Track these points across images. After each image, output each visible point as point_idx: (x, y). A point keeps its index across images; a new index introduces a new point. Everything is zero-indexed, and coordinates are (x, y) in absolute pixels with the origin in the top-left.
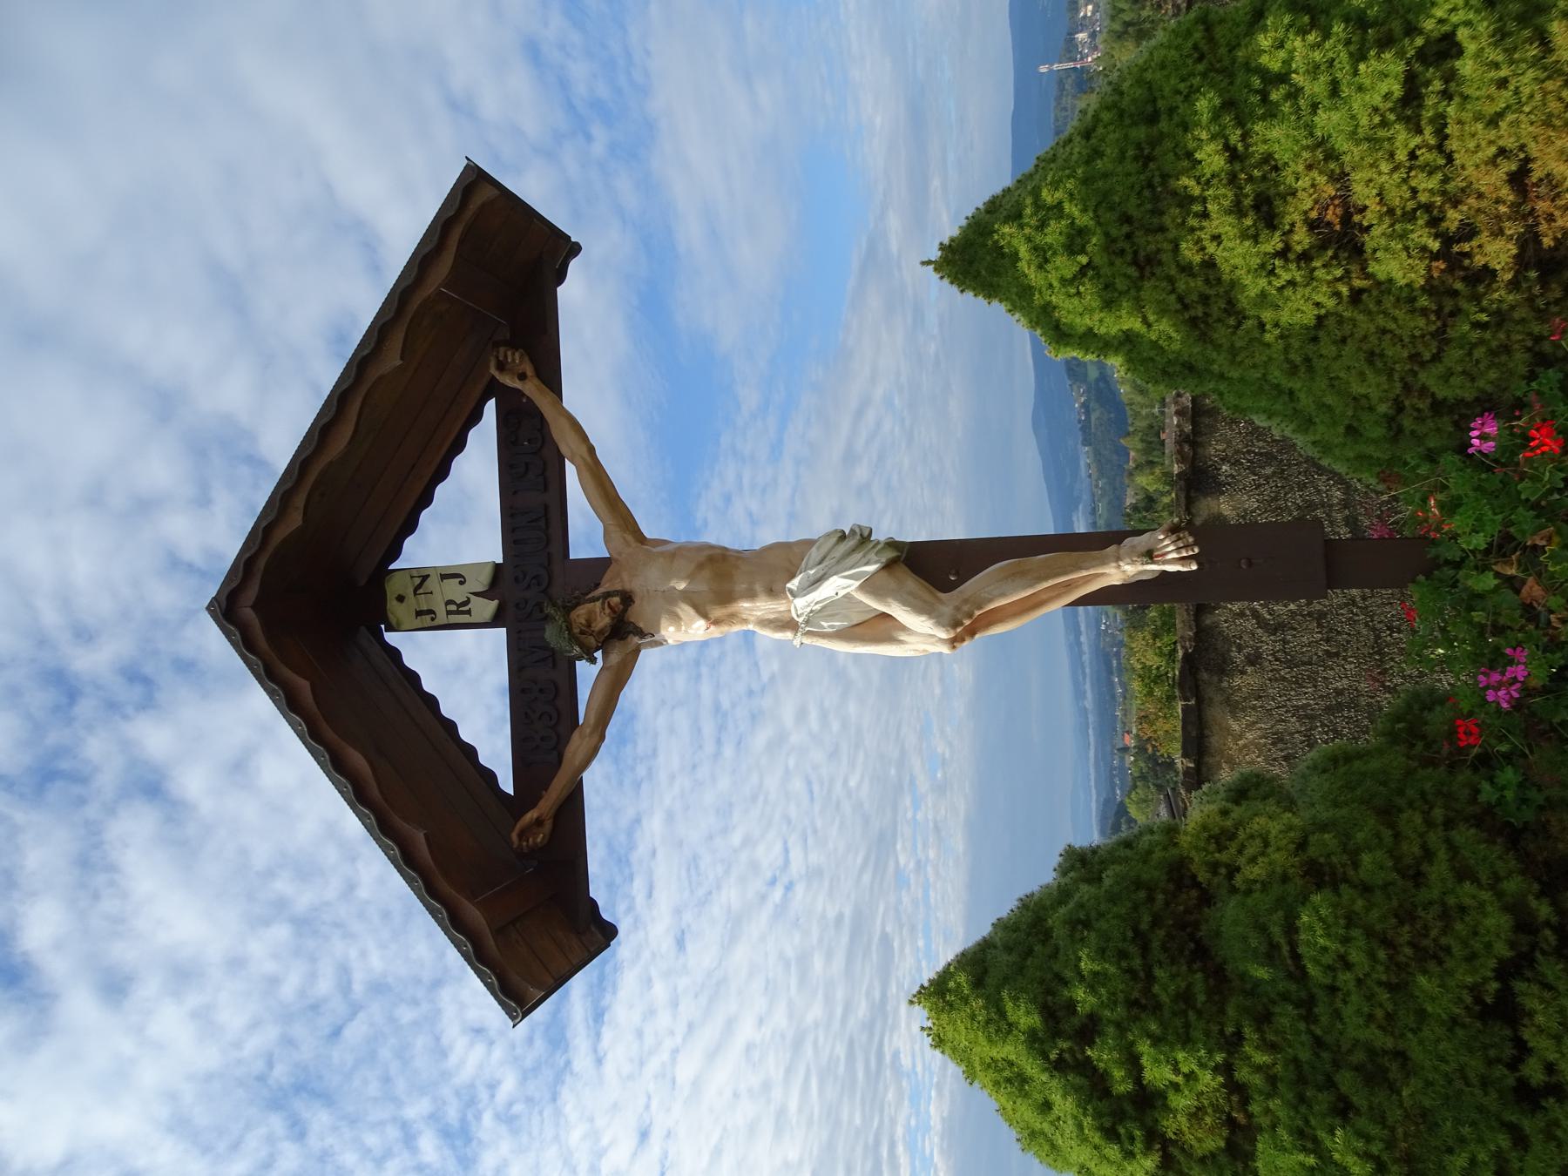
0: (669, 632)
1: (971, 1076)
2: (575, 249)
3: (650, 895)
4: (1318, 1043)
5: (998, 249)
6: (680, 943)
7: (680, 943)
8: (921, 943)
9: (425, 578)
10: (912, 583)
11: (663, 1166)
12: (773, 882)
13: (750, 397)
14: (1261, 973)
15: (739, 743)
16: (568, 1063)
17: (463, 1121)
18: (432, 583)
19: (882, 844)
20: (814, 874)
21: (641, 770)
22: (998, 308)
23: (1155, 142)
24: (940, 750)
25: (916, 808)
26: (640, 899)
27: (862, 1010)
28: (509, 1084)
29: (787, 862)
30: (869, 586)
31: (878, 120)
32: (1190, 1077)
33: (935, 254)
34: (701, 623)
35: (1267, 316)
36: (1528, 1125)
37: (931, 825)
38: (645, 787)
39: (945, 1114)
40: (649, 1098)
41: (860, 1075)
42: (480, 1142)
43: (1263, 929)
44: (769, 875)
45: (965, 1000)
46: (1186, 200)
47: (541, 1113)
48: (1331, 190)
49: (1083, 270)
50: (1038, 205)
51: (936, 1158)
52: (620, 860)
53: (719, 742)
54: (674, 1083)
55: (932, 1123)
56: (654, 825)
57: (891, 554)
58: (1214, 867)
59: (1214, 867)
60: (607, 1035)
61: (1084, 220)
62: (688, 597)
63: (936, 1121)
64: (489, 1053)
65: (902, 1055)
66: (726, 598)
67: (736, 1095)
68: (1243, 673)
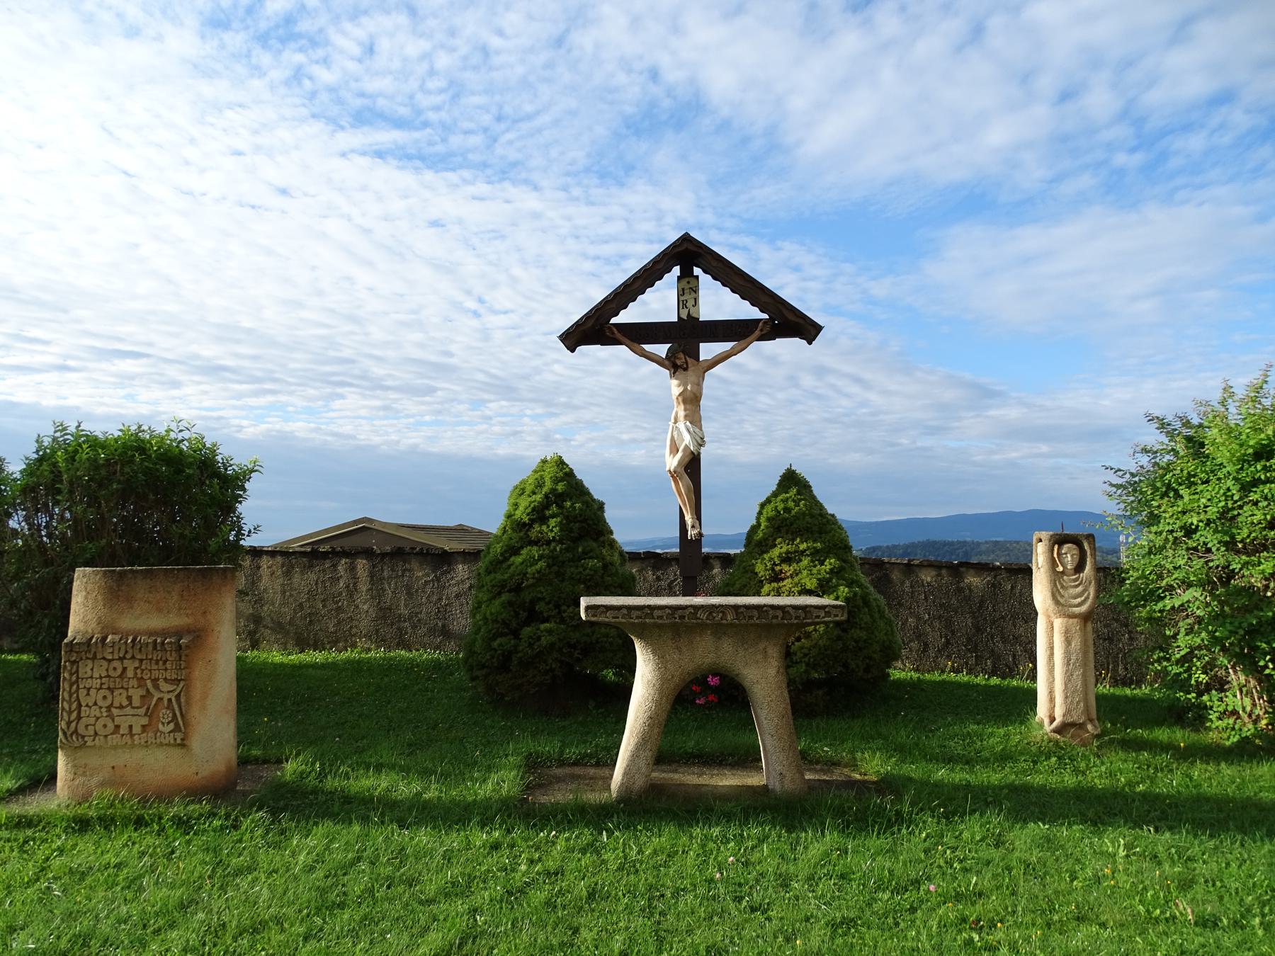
0: (675, 382)
1: (535, 472)
2: (810, 343)
3: (474, 198)
4: (563, 562)
5: (790, 488)
6: (435, 224)
7: (435, 224)
8: (427, 418)
9: (695, 292)
10: (687, 460)
11: (260, 207)
12: (481, 301)
13: (880, 289)
14: (580, 550)
15: (594, 275)
16: (342, 128)
17: (299, 36)
18: (693, 295)
19: (506, 390)
20: (486, 335)
21: (576, 192)
22: (774, 488)
23: (812, 532)
24: (577, 437)
25: (533, 417)
26: (471, 190)
27: (378, 370)
28: (326, 76)
29: (495, 312)
30: (687, 447)
31: (1106, 402)
32: (552, 531)
33: (793, 468)
34: (678, 394)
35: (759, 561)
36: (551, 606)
37: (519, 429)
38: (562, 195)
39: (297, 434)
40: (313, 196)
41: (327, 369)
42: (280, 52)
43: (591, 551)
44: (486, 298)
45: (561, 470)
46: (793, 540)
47: (304, 105)
48: (788, 574)
49: (779, 512)
50: (801, 500)
51: (264, 427)
52: (504, 172)
53: (596, 258)
54: (324, 217)
55: (290, 424)
56: (529, 201)
57: (696, 453)
58: (604, 542)
59: (604, 542)
60: (364, 161)
61: (793, 512)
62: (685, 390)
63: (290, 427)
64: (352, 59)
65: (341, 401)
66: (685, 402)
67: (314, 268)
68: (653, 575)
